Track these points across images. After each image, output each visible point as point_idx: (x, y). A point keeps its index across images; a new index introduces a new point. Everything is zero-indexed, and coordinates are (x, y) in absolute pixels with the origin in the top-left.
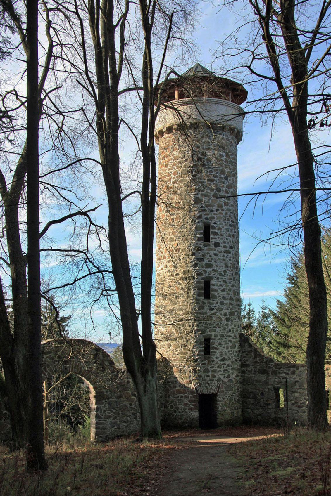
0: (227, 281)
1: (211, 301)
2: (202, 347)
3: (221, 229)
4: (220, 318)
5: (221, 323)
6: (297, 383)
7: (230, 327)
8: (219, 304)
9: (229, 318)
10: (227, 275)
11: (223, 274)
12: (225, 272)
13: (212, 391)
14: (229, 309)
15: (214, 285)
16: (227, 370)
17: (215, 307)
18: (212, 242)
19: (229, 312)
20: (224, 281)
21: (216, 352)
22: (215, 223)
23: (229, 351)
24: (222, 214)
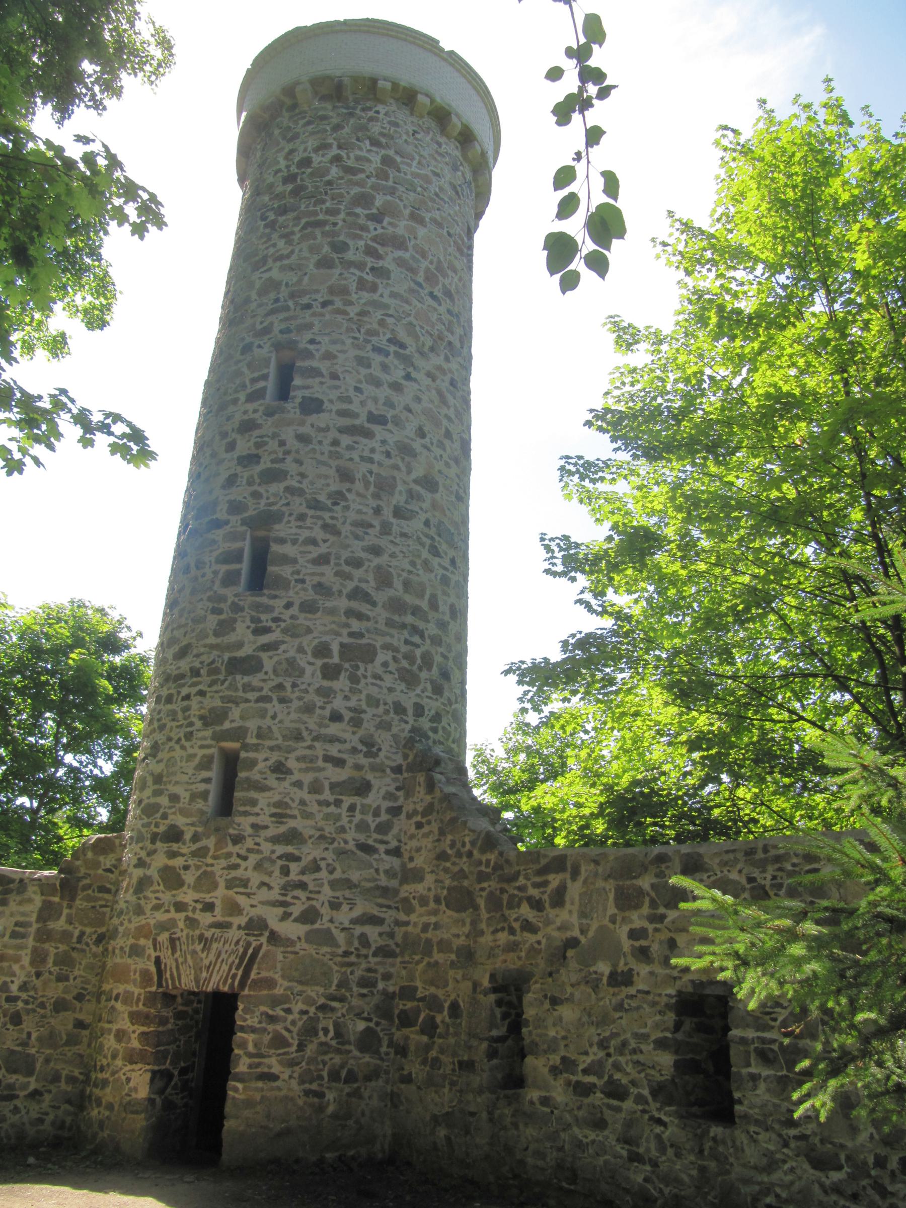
0: (346, 529)
1: (264, 600)
2: (207, 781)
3: (335, 357)
4: (291, 662)
5: (294, 685)
6: (570, 953)
7: (338, 703)
10: (347, 508)
11: (329, 503)
12: (338, 497)
13: (215, 978)
15: (282, 541)
16: (302, 886)
17: (276, 620)
18: (295, 397)
19: (342, 645)
20: (325, 527)
21: (254, 803)
22: (312, 342)
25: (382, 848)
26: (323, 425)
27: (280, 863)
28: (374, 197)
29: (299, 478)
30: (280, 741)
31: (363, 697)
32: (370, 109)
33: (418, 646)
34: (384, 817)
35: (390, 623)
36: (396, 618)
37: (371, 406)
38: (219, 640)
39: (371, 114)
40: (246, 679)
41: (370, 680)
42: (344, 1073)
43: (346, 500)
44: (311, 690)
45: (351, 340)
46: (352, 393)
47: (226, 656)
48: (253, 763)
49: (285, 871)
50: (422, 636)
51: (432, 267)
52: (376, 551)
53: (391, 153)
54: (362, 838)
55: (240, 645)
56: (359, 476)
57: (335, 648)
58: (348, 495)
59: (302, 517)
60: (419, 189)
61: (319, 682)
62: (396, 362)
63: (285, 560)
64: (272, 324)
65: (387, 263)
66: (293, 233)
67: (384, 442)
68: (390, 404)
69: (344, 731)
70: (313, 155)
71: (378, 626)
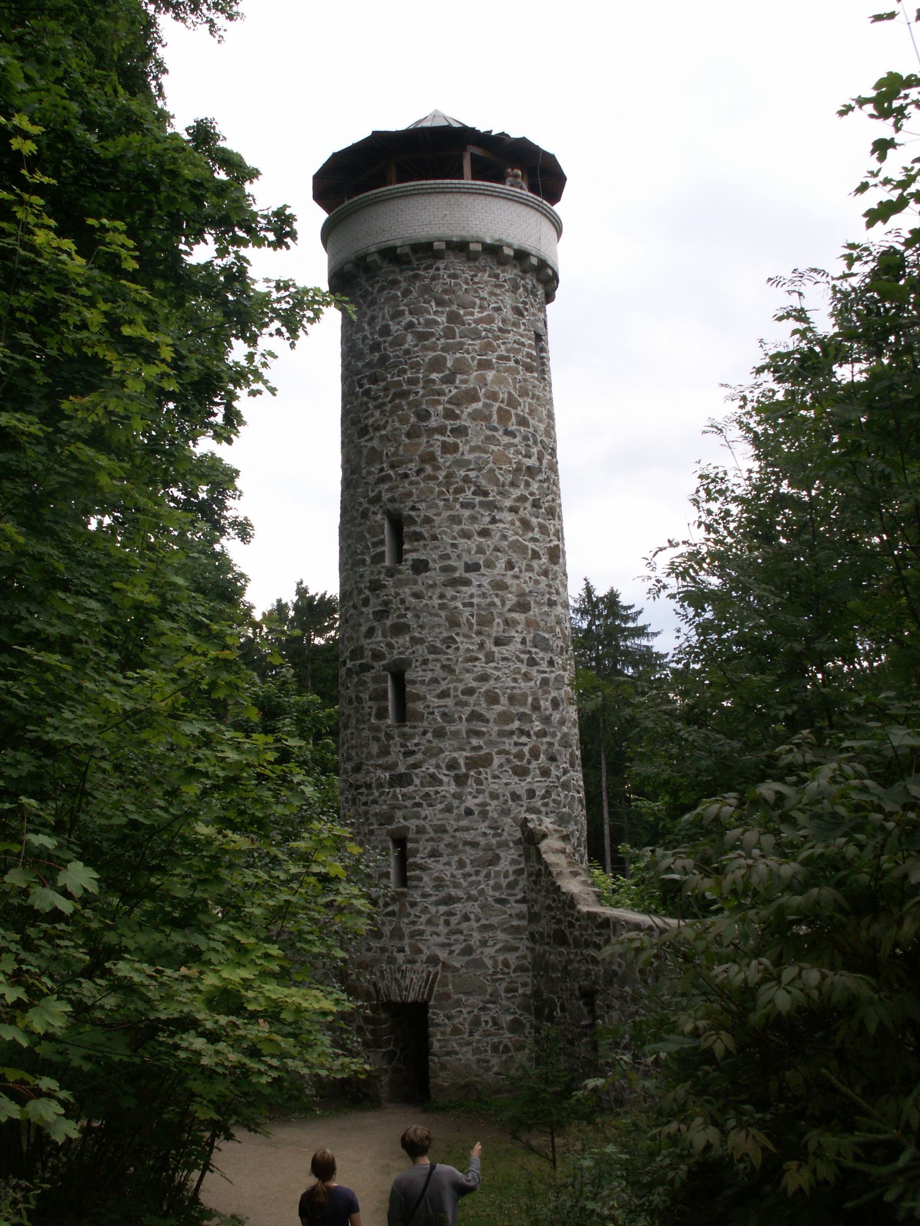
1: (407, 730)
3: (433, 521)
7: (471, 802)
8: (429, 736)
9: (466, 776)
10: (458, 649)
11: (444, 647)
14: (468, 748)
19: (467, 758)
20: (443, 667)
21: (420, 879)
22: (413, 508)
23: (466, 876)
24: (435, 478)
25: (512, 899)
26: (430, 582)
27: (443, 918)
28: (445, 359)
30: (432, 834)
31: (487, 794)
32: (430, 267)
33: (525, 745)
34: (511, 878)
35: (501, 734)
36: (507, 728)
37: (466, 558)
39: (432, 272)
40: (404, 790)
41: (490, 780)
42: (501, 1047)
43: (456, 642)
45: (442, 503)
46: (449, 550)
48: (417, 851)
49: (447, 923)
50: (529, 735)
51: (503, 406)
52: (484, 678)
53: (455, 307)
54: (497, 894)
56: (463, 620)
57: (462, 762)
58: (457, 638)
60: (484, 333)
61: (453, 788)
62: (482, 511)
63: (418, 698)
64: (380, 492)
65: (465, 422)
66: (384, 404)
67: (479, 586)
68: (480, 550)
70: (391, 323)
71: (492, 738)
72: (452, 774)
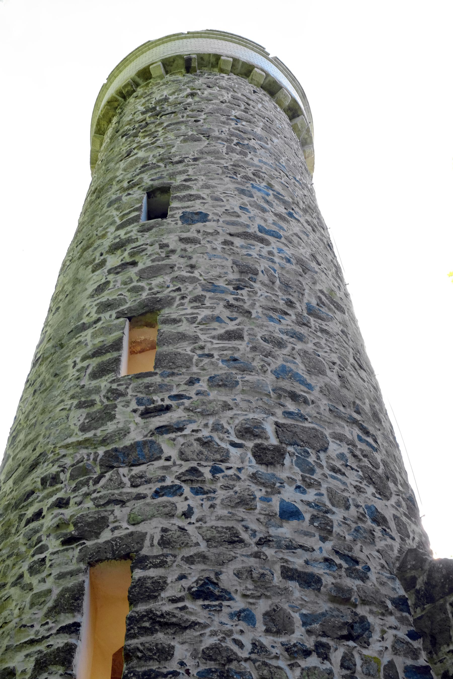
8: (203, 385)
17: (179, 397)
29: (189, 269)
38: (89, 435)
44: (243, 476)
47: (101, 451)
55: (125, 432)
59: (199, 299)
69: (307, 534)
72: (250, 444)
